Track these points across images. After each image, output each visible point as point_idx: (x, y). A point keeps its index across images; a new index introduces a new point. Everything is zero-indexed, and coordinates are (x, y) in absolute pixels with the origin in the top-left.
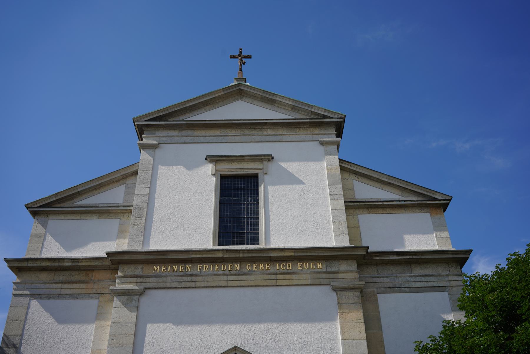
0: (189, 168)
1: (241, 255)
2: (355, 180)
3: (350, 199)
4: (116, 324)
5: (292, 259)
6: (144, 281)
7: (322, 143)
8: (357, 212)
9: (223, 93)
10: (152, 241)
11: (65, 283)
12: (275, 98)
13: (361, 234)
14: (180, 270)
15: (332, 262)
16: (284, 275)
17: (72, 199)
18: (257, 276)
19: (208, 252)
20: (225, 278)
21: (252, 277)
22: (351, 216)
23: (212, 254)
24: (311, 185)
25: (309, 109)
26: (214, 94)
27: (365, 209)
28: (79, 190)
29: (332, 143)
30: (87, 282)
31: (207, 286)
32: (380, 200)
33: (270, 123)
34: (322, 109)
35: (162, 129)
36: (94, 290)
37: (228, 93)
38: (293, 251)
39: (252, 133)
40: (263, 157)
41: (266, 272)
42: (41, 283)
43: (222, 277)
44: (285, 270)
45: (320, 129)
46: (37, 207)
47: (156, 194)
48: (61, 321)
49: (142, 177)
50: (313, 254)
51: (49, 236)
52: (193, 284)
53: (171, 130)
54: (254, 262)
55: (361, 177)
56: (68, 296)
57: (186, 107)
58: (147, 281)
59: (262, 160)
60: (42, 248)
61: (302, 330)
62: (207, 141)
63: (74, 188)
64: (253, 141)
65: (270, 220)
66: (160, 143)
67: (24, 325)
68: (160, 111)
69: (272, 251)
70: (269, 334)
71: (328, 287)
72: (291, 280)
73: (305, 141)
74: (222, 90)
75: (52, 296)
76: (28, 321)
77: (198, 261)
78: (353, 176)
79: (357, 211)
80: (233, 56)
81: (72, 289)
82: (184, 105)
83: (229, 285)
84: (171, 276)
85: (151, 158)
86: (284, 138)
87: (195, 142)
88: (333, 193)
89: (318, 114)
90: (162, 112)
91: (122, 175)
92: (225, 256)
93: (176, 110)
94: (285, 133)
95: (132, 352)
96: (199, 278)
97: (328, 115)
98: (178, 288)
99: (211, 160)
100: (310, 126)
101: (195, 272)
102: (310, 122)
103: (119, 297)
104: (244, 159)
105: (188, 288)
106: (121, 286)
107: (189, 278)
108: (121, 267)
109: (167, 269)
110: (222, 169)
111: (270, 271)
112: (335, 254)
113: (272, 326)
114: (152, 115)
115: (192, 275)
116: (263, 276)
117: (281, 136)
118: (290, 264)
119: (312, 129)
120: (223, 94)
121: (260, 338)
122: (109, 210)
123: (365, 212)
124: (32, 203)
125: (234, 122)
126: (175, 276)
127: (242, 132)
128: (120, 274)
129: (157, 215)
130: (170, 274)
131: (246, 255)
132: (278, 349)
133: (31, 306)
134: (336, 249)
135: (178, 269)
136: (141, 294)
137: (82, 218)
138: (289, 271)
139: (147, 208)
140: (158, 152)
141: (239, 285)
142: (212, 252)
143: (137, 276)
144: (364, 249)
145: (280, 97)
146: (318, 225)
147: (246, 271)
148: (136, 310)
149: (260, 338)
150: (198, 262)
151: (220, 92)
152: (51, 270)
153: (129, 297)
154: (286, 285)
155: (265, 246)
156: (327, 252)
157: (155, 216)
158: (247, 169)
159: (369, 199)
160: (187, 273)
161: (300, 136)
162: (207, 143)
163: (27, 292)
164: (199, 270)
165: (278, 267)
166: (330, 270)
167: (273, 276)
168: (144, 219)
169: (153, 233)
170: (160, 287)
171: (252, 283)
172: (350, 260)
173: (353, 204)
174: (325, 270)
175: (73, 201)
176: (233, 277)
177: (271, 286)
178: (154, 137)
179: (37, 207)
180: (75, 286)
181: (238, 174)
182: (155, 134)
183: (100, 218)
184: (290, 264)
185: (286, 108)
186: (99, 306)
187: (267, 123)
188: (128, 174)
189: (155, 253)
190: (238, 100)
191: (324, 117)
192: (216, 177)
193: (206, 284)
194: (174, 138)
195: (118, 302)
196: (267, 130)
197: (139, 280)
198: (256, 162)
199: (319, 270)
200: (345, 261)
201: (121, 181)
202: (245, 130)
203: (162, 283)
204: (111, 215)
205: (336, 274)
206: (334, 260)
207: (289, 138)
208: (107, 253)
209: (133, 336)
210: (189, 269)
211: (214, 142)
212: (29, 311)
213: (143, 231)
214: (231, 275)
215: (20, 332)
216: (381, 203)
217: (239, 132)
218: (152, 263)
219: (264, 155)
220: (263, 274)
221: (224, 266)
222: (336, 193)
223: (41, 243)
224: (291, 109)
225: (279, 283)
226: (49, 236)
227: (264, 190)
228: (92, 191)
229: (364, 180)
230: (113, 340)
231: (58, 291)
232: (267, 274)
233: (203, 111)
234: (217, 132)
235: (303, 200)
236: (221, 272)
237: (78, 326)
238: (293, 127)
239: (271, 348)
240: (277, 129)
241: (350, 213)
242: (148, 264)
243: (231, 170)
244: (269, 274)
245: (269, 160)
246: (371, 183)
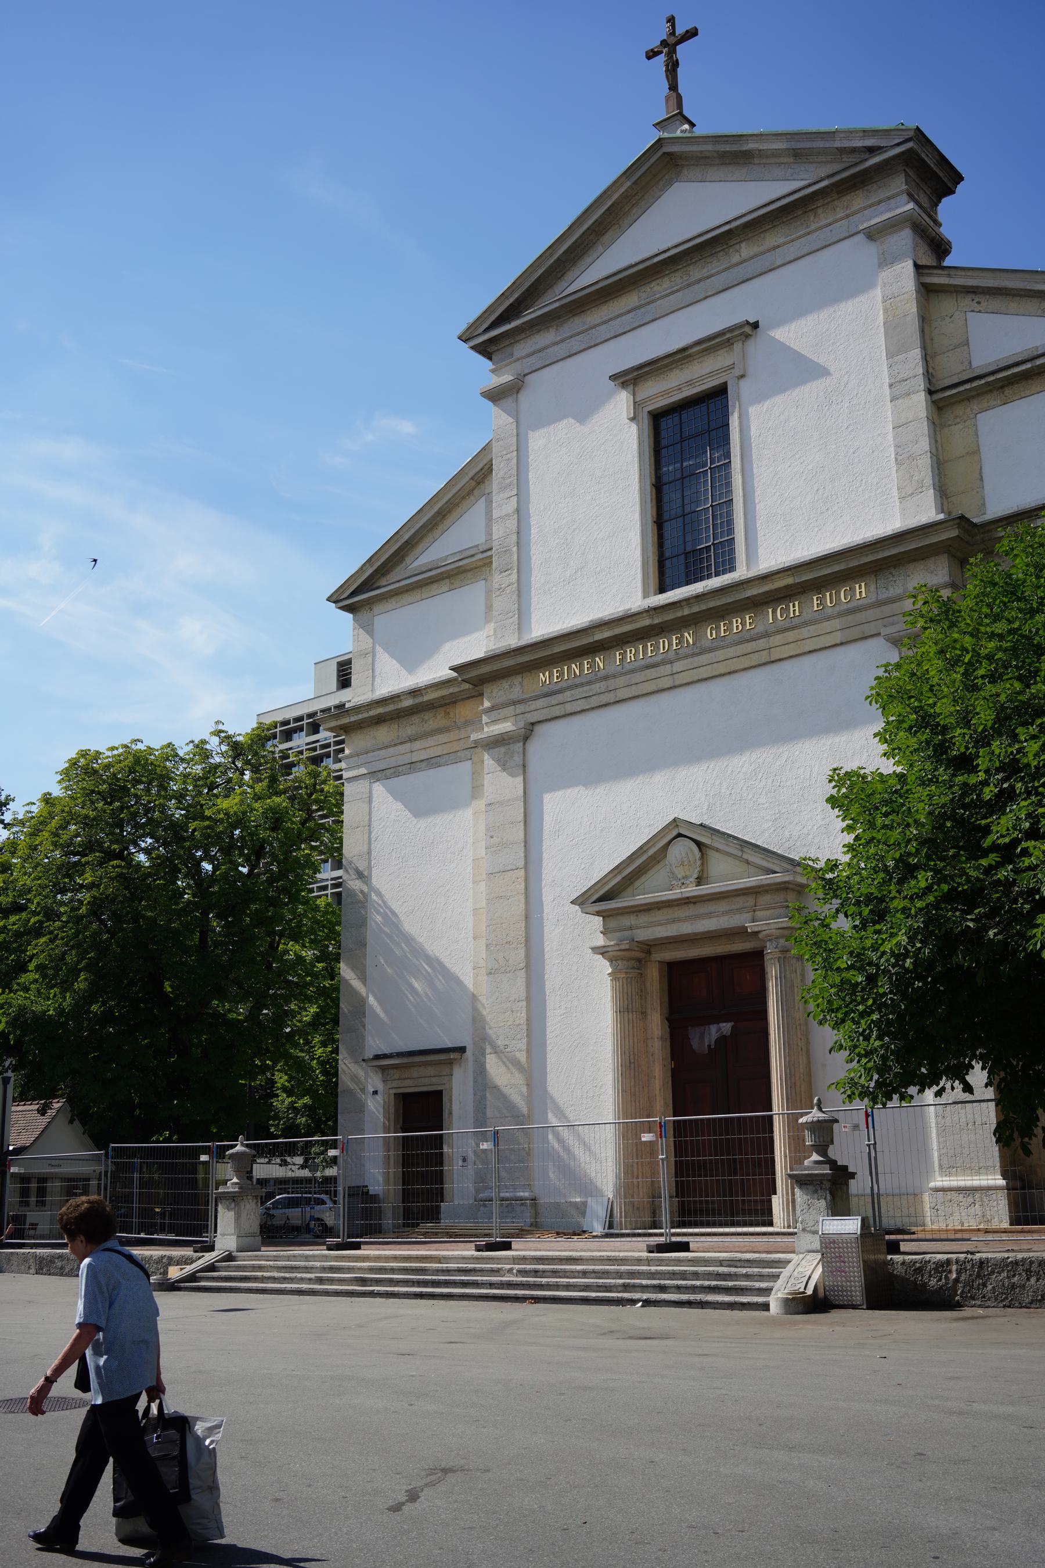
0: (582, 417)
1: (686, 611)
2: (973, 311)
3: (956, 376)
4: (493, 807)
5: (799, 590)
6: (528, 710)
7: (872, 235)
8: (975, 407)
9: (628, 184)
10: (535, 617)
11: (415, 740)
12: (745, 148)
13: (983, 471)
14: (586, 672)
15: (891, 573)
16: (785, 634)
17: (402, 559)
18: (729, 649)
19: (622, 622)
20: (667, 669)
21: (720, 655)
22: (957, 427)
23: (631, 622)
24: (847, 372)
25: (828, 145)
26: (610, 197)
27: (995, 393)
28: (406, 537)
29: (895, 226)
30: (446, 730)
31: (637, 694)
32: (1035, 353)
33: (737, 227)
34: (857, 131)
35: (523, 335)
36: (462, 742)
37: (640, 177)
38: (789, 572)
39: (705, 270)
40: (728, 335)
41: (747, 637)
42: (381, 749)
43: (662, 668)
44: (787, 619)
45: (867, 190)
46: (348, 598)
47: (531, 506)
48: (419, 811)
49: (501, 474)
50: (836, 568)
51: (379, 649)
52: (611, 697)
53: (541, 333)
54: (722, 617)
55: (988, 297)
56: (424, 764)
57: (558, 259)
58: (532, 708)
59: (728, 343)
60: (374, 677)
61: (826, 755)
62: (612, 335)
63: (395, 538)
64: (710, 294)
65: (757, 501)
66: (525, 375)
67: (370, 833)
68: (506, 294)
69: (744, 586)
70: (761, 774)
71: (880, 641)
72: (799, 643)
73: (830, 245)
74: (624, 178)
75: (400, 769)
76: (374, 824)
77: (615, 643)
78: (967, 302)
79: (975, 406)
80: (652, 50)
81: (428, 750)
82: (551, 255)
83: (677, 683)
84: (570, 688)
85: (512, 420)
86: (779, 256)
87: (589, 345)
88: (900, 377)
89: (854, 150)
90: (511, 294)
91: (472, 478)
92: (656, 621)
93: (540, 277)
94: (782, 240)
95: (523, 855)
96: (621, 681)
97: (876, 144)
98: (588, 710)
99: (623, 383)
100: (838, 193)
101: (611, 670)
102: (831, 185)
103: (491, 750)
104: (690, 356)
105: (606, 705)
106: (492, 728)
107: (601, 686)
108: (487, 689)
109: (561, 674)
110: (649, 399)
111: (756, 631)
112: (886, 554)
113: (764, 756)
114: (493, 312)
115: (606, 678)
116: (741, 646)
117: (773, 252)
118: (863, 584)
119: (846, 199)
120: (630, 187)
121: (744, 788)
122: (460, 567)
123: (994, 403)
124: (336, 591)
125: (656, 260)
126: (577, 686)
127: (685, 278)
128: (487, 704)
129: (537, 554)
130: (570, 683)
131: (696, 609)
132: (779, 805)
133: (375, 796)
134: (886, 543)
135: (581, 670)
136: (527, 734)
137: (424, 596)
138: (796, 621)
139: (518, 544)
140: (525, 397)
141: (696, 678)
142: (630, 619)
143: (514, 703)
144: (951, 523)
145: (755, 138)
146: (864, 481)
147: (708, 644)
148: (522, 772)
149: (744, 788)
150: (615, 646)
151: (622, 185)
152: (392, 719)
153: (507, 747)
154: (791, 657)
155: (745, 572)
156: (867, 555)
157: (534, 558)
158: (702, 378)
159: (1006, 358)
160: (598, 673)
161: (817, 233)
162: (615, 337)
163: (363, 771)
164: (618, 663)
165: (772, 616)
166: (883, 595)
167: (761, 641)
168: (516, 571)
169: (534, 600)
170: (555, 715)
171: (722, 668)
172: (933, 558)
173: (954, 391)
174: (873, 598)
175: (404, 564)
176: (682, 662)
177: (760, 665)
178: (511, 363)
179: (348, 598)
180: (431, 741)
181: (686, 398)
182: (512, 355)
183: (453, 587)
184: (863, 584)
185: (781, 160)
186: (473, 773)
187: (730, 231)
188: (483, 471)
189: (529, 649)
190: (670, 183)
191: (872, 150)
192: (638, 425)
193: (634, 691)
194: (548, 351)
195: (492, 762)
196: (740, 248)
197: (520, 708)
198: (719, 352)
199: (860, 602)
200: (922, 562)
201: (476, 492)
202: (691, 267)
203: (557, 707)
204: (469, 574)
205: (898, 603)
206: (895, 567)
207: (792, 250)
208: (454, 669)
209: (522, 824)
210: (691, 641)
211: (629, 328)
212: (373, 805)
213: (516, 599)
214: (678, 659)
215: (365, 849)
216: (1028, 366)
217: (678, 280)
218: (591, 653)
219: (731, 329)
220: (740, 643)
221: (664, 642)
222: (906, 376)
223: (370, 667)
224: (791, 160)
225: (776, 654)
226: (379, 649)
227: (741, 424)
228: (431, 530)
229: (996, 303)
230: (492, 837)
231: (407, 759)
232: (748, 641)
233: (600, 248)
234: (631, 299)
235: (828, 421)
236: (659, 658)
237: (448, 817)
238: (800, 212)
239: (766, 806)
240: (762, 235)
241: (956, 417)
242: (530, 671)
243: (667, 393)
244: (753, 639)
245: (748, 336)
246: (1013, 305)
